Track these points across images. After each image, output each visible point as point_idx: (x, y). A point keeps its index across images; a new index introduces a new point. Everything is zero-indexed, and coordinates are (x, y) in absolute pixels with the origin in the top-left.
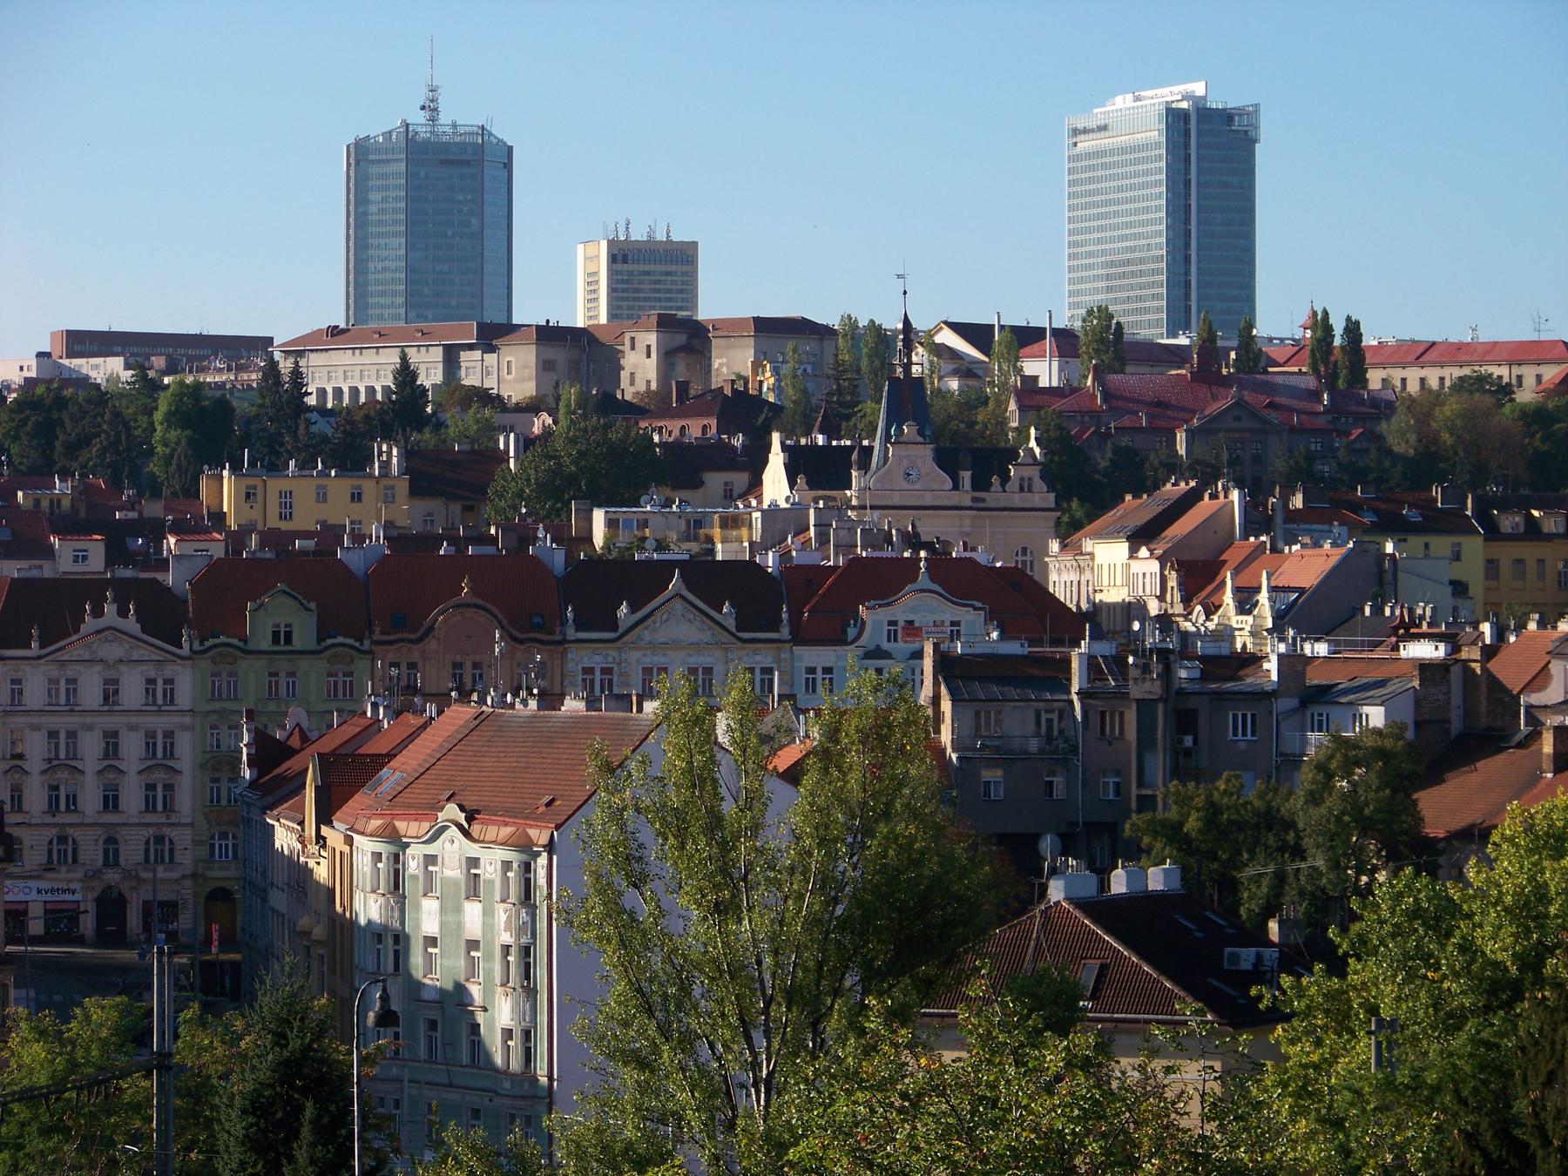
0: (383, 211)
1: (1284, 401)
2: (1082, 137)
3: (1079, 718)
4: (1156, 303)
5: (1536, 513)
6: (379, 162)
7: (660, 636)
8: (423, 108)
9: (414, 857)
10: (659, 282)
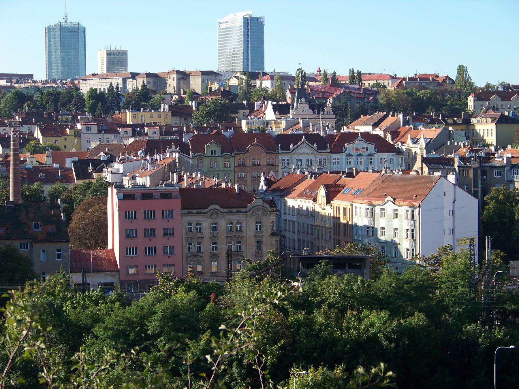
0: (55, 43)
1: (352, 91)
2: (221, 24)
3: (458, 172)
4: (241, 64)
5: (455, 119)
6: (54, 31)
7: (300, 152)
8: (64, 18)
9: (377, 210)
10: (118, 60)
